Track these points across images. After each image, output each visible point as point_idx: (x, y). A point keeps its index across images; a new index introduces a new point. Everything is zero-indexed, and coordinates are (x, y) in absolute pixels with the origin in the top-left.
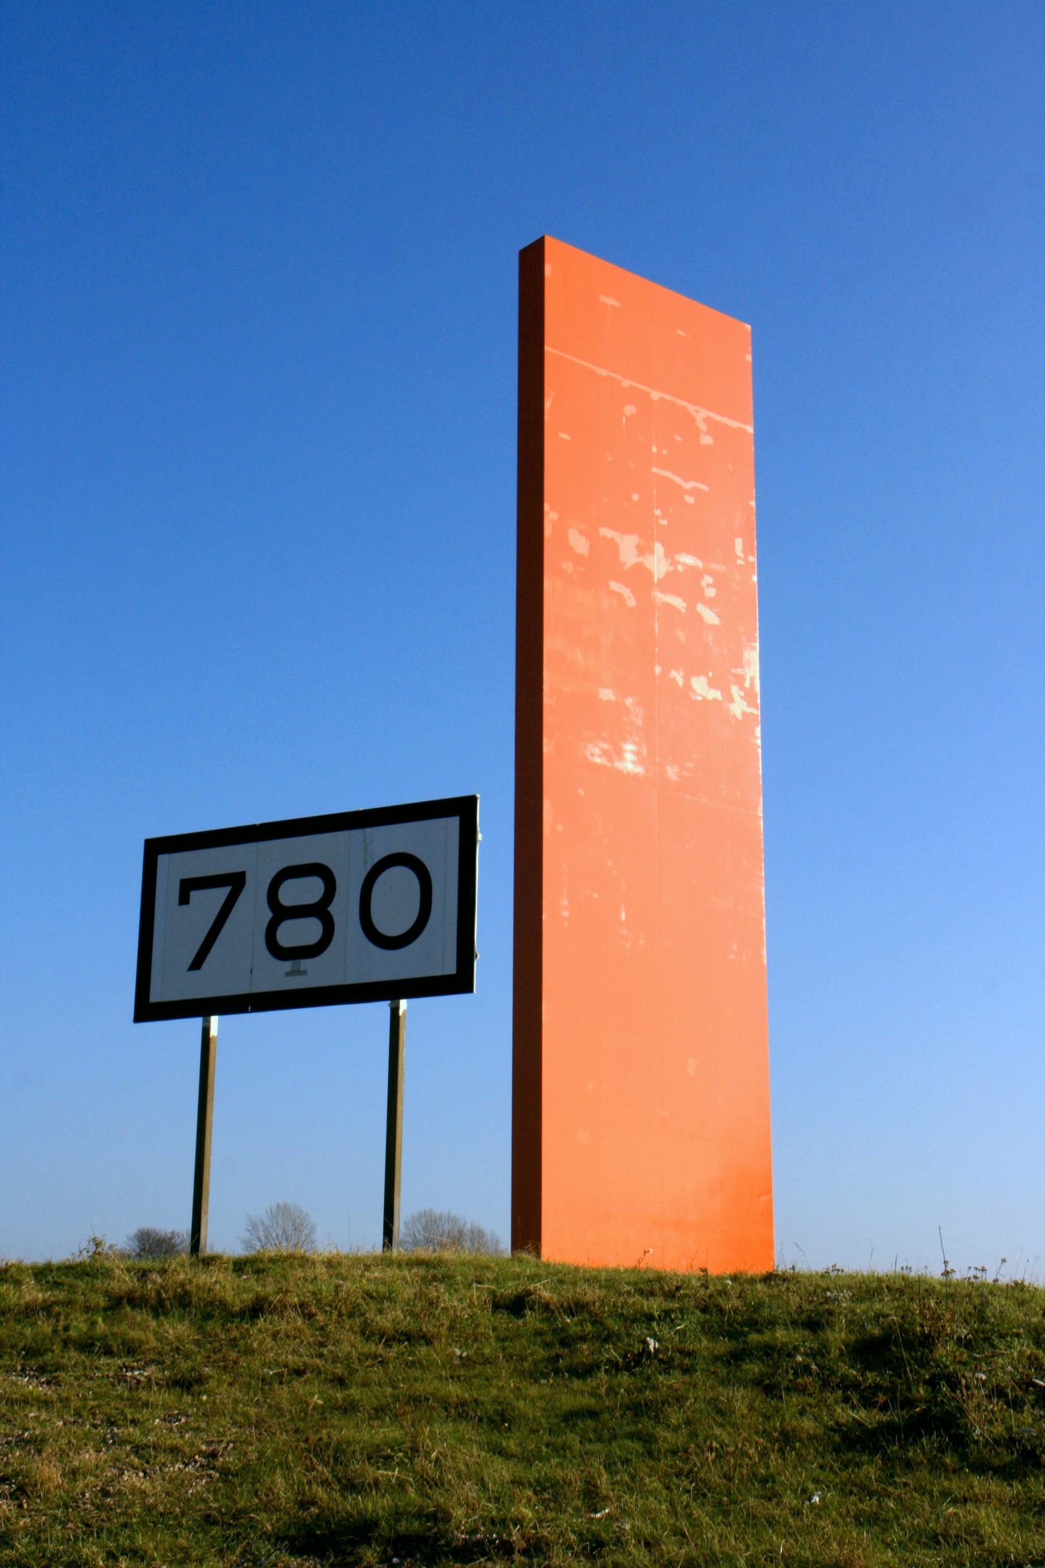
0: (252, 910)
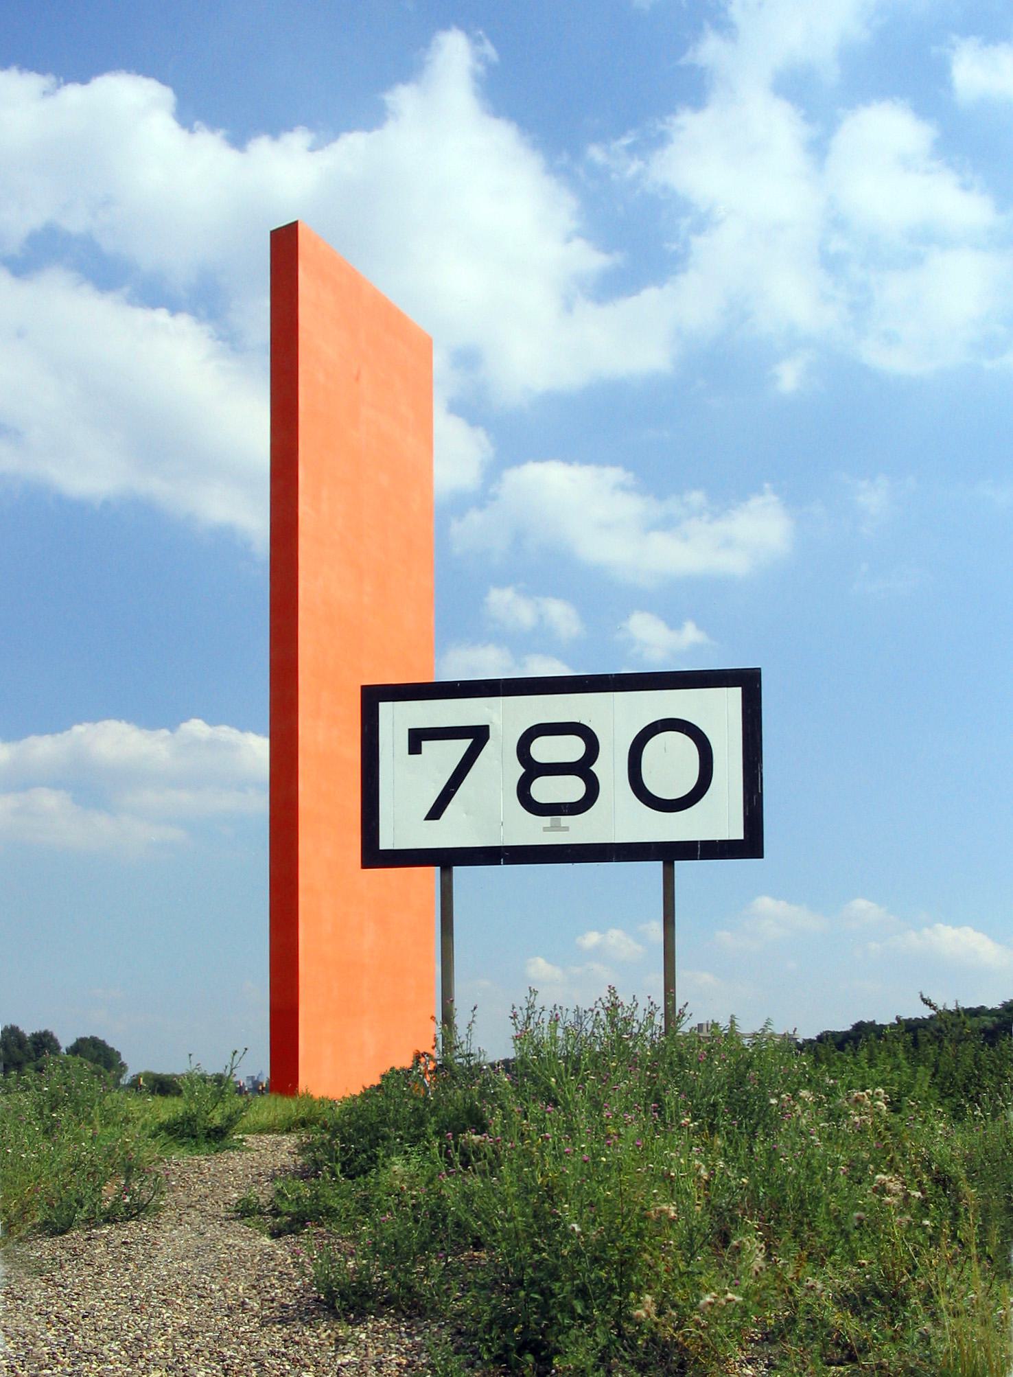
0: (498, 767)
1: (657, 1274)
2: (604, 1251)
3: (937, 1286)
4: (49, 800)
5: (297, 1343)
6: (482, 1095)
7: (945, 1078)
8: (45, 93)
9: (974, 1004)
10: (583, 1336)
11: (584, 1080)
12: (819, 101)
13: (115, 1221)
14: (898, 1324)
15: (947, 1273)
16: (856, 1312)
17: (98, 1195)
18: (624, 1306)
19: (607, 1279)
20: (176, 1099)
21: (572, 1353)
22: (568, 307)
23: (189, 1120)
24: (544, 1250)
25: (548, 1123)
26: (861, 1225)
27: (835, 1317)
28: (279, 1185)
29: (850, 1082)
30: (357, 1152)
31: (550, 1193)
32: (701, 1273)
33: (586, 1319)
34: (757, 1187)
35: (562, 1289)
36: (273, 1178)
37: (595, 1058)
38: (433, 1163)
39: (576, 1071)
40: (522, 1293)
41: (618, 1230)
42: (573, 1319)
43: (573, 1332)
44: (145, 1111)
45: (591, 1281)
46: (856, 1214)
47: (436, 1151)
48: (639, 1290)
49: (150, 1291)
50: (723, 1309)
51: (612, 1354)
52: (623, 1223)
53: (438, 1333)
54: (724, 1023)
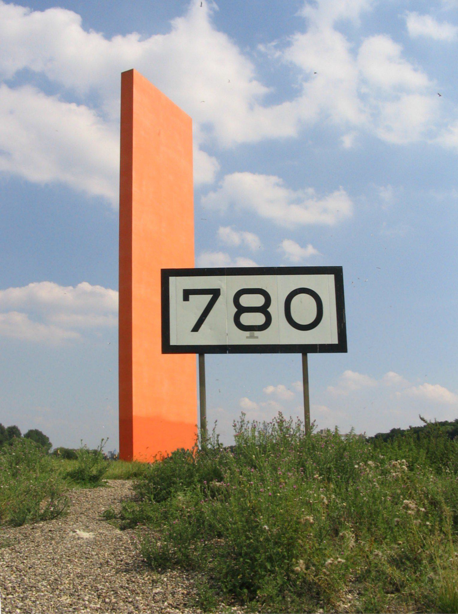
0: (224, 308)
1: (305, 550)
2: (280, 539)
3: (434, 554)
4: (18, 318)
5: (134, 582)
6: (220, 463)
7: (432, 454)
8: (25, 15)
9: (442, 420)
10: (271, 580)
11: (268, 456)
12: (353, 33)
13: (46, 520)
14: (418, 574)
15: (439, 548)
16: (398, 567)
17: (37, 506)
18: (290, 565)
19: (281, 552)
20: (75, 461)
21: (266, 588)
22: (251, 108)
23: (81, 471)
24: (251, 538)
25: (252, 477)
26: (398, 524)
27: (389, 570)
28: (124, 504)
29: (390, 457)
30: (161, 490)
31: (254, 511)
32: (325, 549)
33: (272, 572)
34: (350, 507)
35: (261, 557)
36: (121, 501)
37: (273, 446)
38: (197, 495)
39: (265, 452)
40: (241, 559)
41: (286, 529)
42: (266, 571)
43: (266, 578)
44: (60, 466)
45: (274, 554)
46: (396, 519)
47: (199, 490)
48: (297, 558)
49: (62, 555)
50: (336, 566)
51: (285, 588)
52: (288, 525)
53: (202, 578)
54: (333, 430)
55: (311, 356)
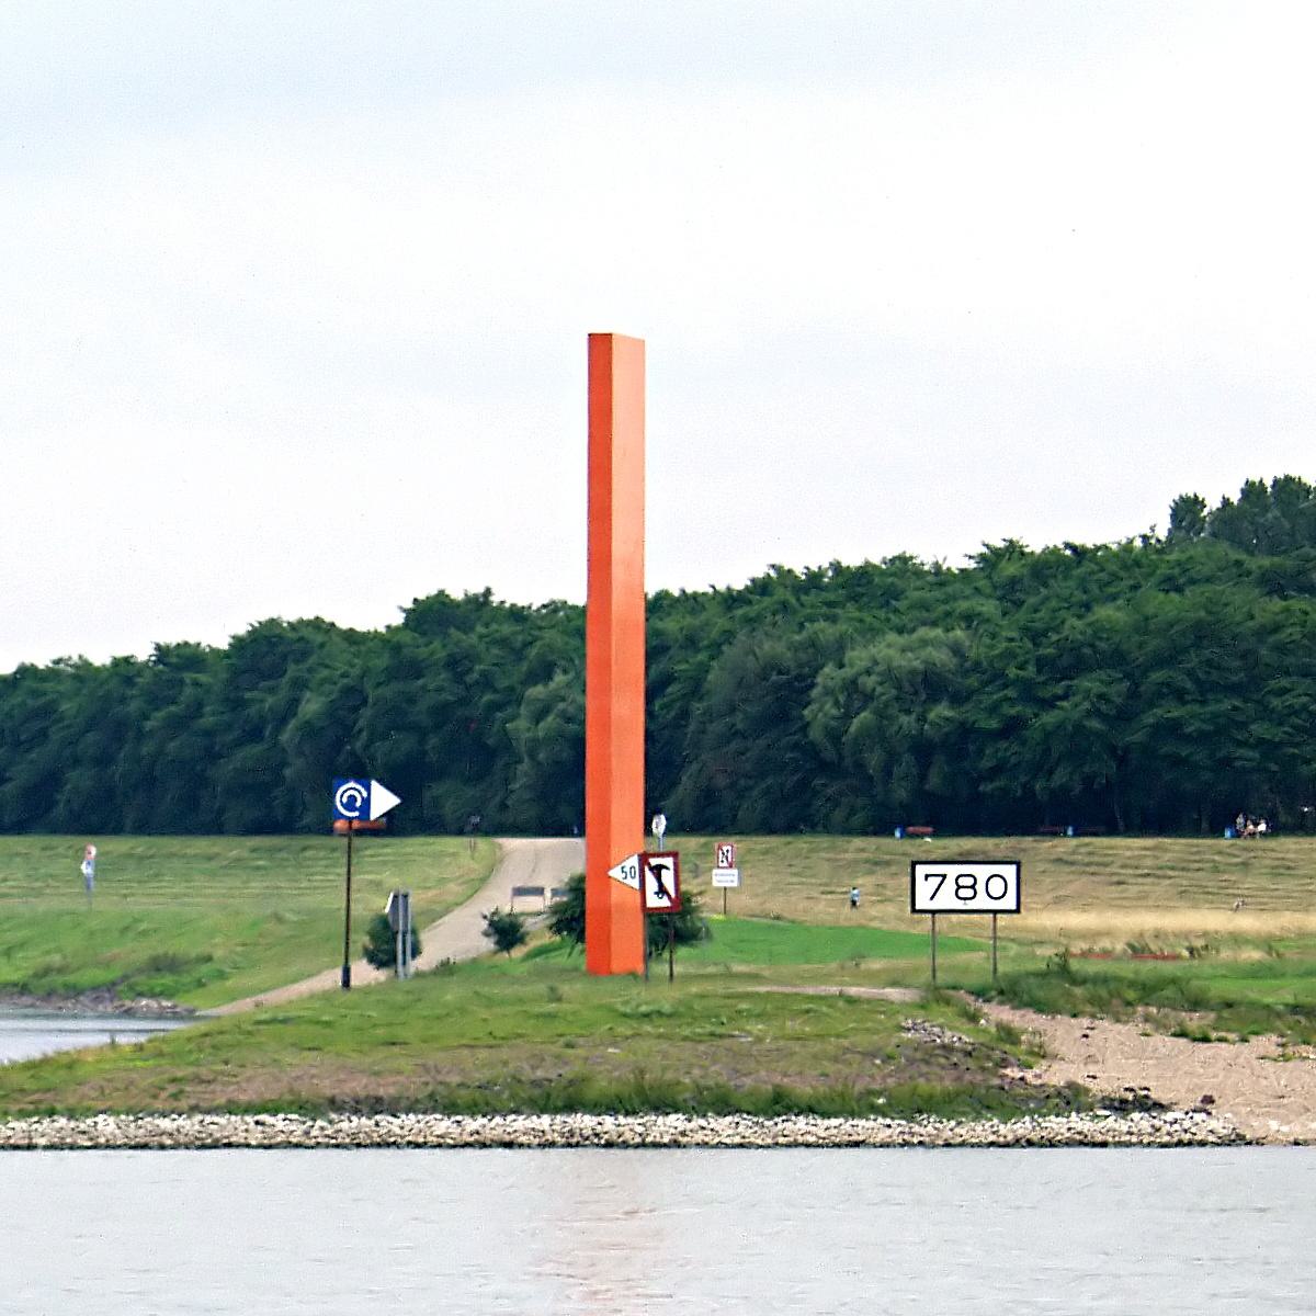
0: (950, 885)
55: (999, 916)
